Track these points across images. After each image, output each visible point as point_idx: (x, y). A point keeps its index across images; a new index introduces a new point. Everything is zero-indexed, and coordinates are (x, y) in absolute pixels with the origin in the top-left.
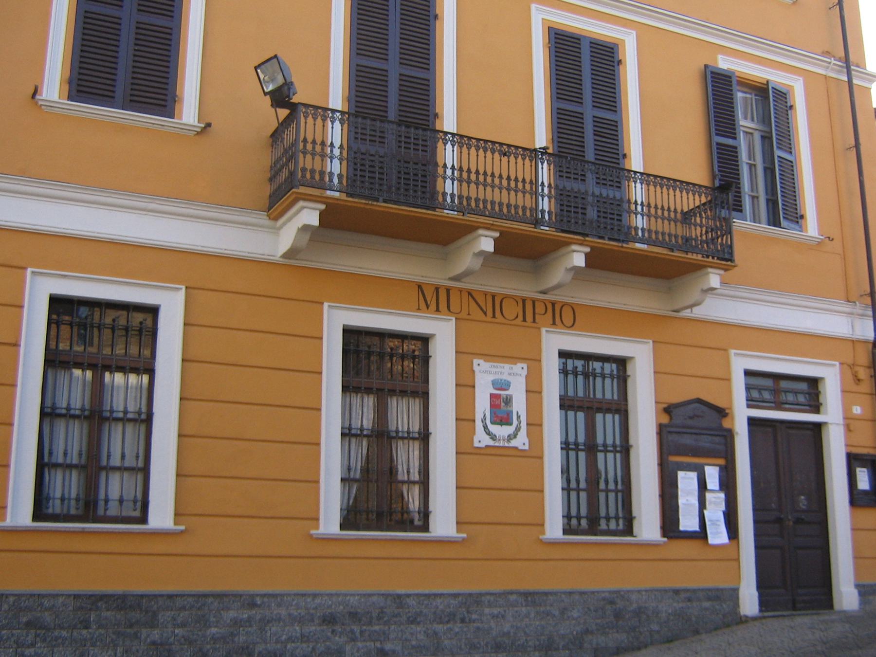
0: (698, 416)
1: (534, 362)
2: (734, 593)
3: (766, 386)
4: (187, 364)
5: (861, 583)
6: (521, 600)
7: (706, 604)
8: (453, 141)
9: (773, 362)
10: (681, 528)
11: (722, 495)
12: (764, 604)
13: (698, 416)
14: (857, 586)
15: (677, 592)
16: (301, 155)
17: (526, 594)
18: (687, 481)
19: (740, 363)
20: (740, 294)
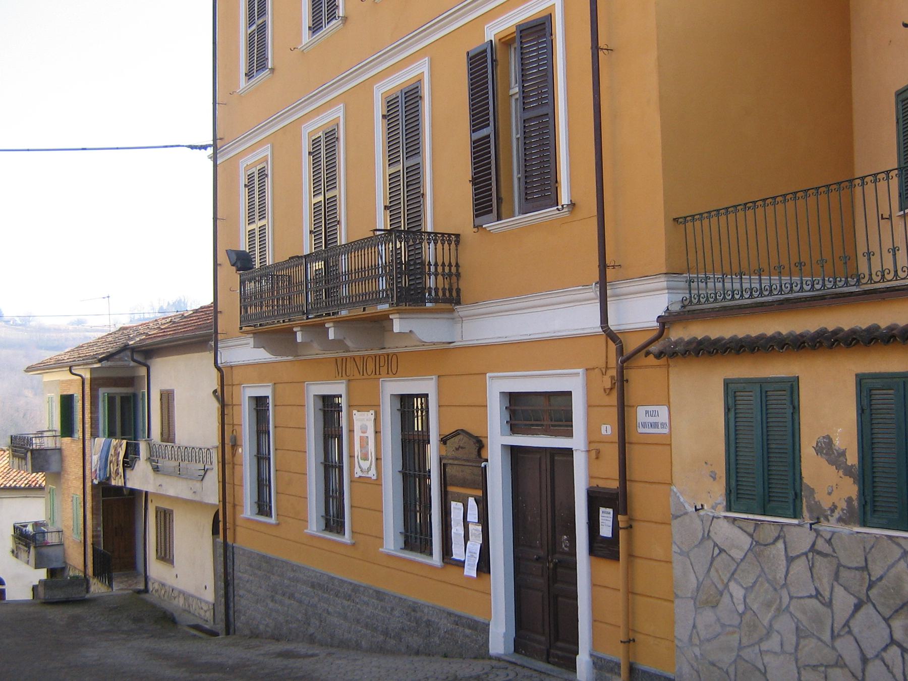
0: (462, 448)
1: (375, 406)
2: (483, 629)
3: (523, 410)
4: (442, 409)
5: (595, 654)
6: (374, 594)
7: (468, 631)
8: (429, 239)
9: (527, 380)
10: (610, 535)
11: (480, 528)
12: (521, 644)
13: (462, 448)
14: (591, 655)
15: (450, 614)
16: (427, 277)
17: (378, 592)
18: (456, 509)
19: (499, 385)
20: (489, 310)
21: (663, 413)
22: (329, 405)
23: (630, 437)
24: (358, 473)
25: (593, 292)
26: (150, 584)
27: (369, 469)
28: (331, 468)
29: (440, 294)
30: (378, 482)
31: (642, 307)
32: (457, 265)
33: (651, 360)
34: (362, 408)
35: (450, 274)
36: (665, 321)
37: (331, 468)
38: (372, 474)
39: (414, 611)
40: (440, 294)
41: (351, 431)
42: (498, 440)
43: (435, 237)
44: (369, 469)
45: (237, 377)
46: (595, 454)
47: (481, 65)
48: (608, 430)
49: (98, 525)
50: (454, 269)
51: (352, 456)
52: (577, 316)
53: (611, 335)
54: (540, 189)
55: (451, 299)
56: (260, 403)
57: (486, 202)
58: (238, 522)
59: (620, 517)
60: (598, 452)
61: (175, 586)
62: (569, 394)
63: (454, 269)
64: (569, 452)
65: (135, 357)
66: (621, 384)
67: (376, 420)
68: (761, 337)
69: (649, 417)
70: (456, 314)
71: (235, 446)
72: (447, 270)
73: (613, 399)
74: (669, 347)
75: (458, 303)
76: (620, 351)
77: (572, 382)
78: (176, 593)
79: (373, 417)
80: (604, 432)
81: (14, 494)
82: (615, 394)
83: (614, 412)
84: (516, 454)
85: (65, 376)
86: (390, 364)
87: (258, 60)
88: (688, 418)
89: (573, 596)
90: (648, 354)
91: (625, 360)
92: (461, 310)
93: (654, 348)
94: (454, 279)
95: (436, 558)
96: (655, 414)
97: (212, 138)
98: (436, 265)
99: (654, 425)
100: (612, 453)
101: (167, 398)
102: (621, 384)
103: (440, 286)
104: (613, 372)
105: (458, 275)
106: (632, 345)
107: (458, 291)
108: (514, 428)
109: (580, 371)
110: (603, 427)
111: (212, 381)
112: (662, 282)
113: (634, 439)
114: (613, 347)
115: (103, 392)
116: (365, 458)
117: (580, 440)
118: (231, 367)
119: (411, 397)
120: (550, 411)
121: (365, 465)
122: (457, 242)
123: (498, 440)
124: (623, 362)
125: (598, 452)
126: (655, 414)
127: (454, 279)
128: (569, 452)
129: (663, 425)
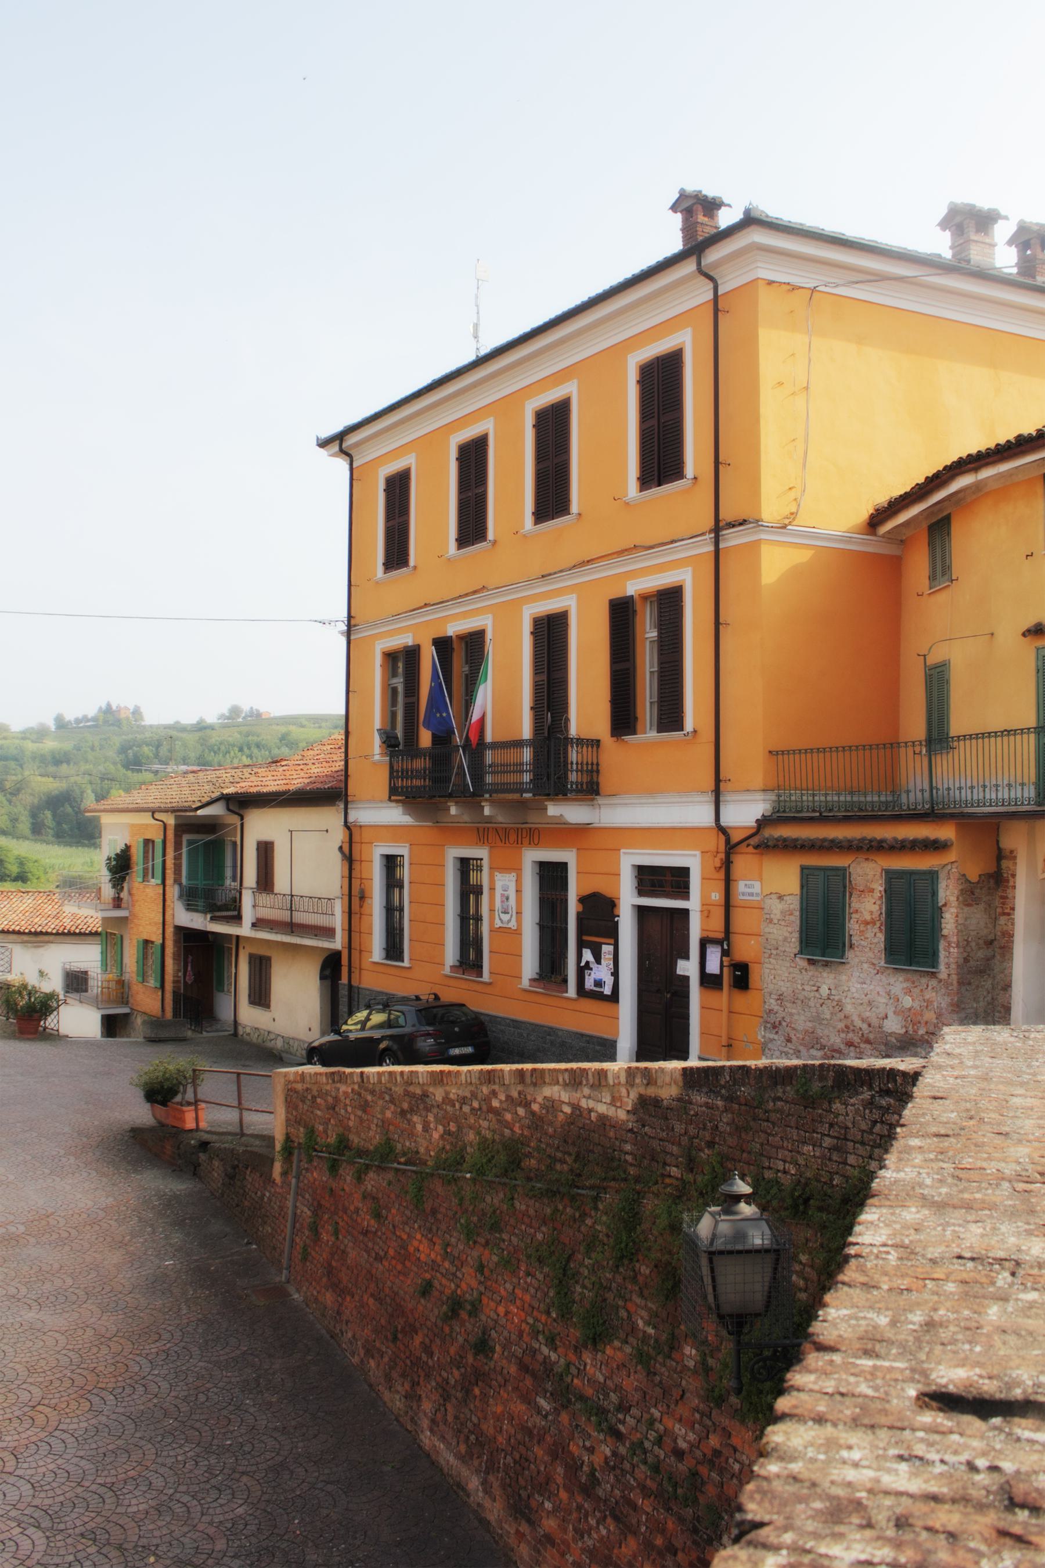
1: (518, 870)
3: (651, 879)
7: (598, 1048)
19: (628, 861)
21: (757, 887)
22: (465, 865)
23: (732, 902)
24: (498, 924)
25: (710, 797)
26: (240, 1028)
27: (509, 921)
28: (469, 920)
29: (585, 787)
30: (518, 932)
31: (744, 812)
32: (598, 764)
33: (751, 849)
34: (505, 869)
35: (592, 771)
36: (763, 823)
37: (469, 920)
38: (513, 924)
39: (549, 1035)
40: (585, 787)
41: (492, 889)
42: (628, 900)
43: (580, 742)
44: (509, 921)
45: (366, 836)
46: (706, 914)
47: (622, 613)
48: (717, 896)
49: (179, 971)
50: (595, 767)
51: (492, 910)
52: (697, 813)
53: (722, 830)
54: (670, 716)
55: (591, 789)
56: (391, 862)
57: (623, 720)
58: (364, 966)
59: (724, 958)
60: (709, 912)
61: (271, 1029)
62: (566, 864)
63: (595, 767)
64: (685, 912)
65: (231, 807)
66: (727, 865)
67: (519, 881)
68: (824, 840)
69: (747, 888)
70: (595, 802)
71: (362, 898)
72: (590, 767)
73: (722, 875)
74: (764, 840)
75: (598, 793)
76: (728, 841)
77: (691, 860)
78: (272, 1036)
79: (514, 879)
80: (713, 898)
81: (68, 939)
82: (723, 870)
83: (721, 885)
84: (642, 912)
85: (146, 819)
86: (533, 836)
87: (397, 555)
88: (772, 890)
89: (686, 1017)
90: (748, 845)
91: (729, 847)
92: (600, 800)
93: (754, 841)
94: (595, 774)
95: (572, 991)
96: (753, 886)
97: (346, 615)
98: (577, 764)
99: (752, 894)
100: (719, 914)
101: (266, 850)
102: (727, 865)
103: (585, 781)
104: (722, 856)
105: (598, 771)
106: (736, 837)
107: (598, 784)
108: (641, 892)
109: (698, 853)
110: (713, 895)
111: (339, 836)
112: (759, 796)
113: (736, 904)
114: (722, 838)
115: (185, 838)
116: (506, 912)
117: (697, 903)
118: (361, 826)
119: (468, 859)
120: (676, 881)
121: (505, 917)
122: (598, 746)
123: (628, 900)
124: (730, 849)
125: (709, 912)
126: (753, 886)
127: (595, 774)
128: (685, 912)
129: (757, 894)
